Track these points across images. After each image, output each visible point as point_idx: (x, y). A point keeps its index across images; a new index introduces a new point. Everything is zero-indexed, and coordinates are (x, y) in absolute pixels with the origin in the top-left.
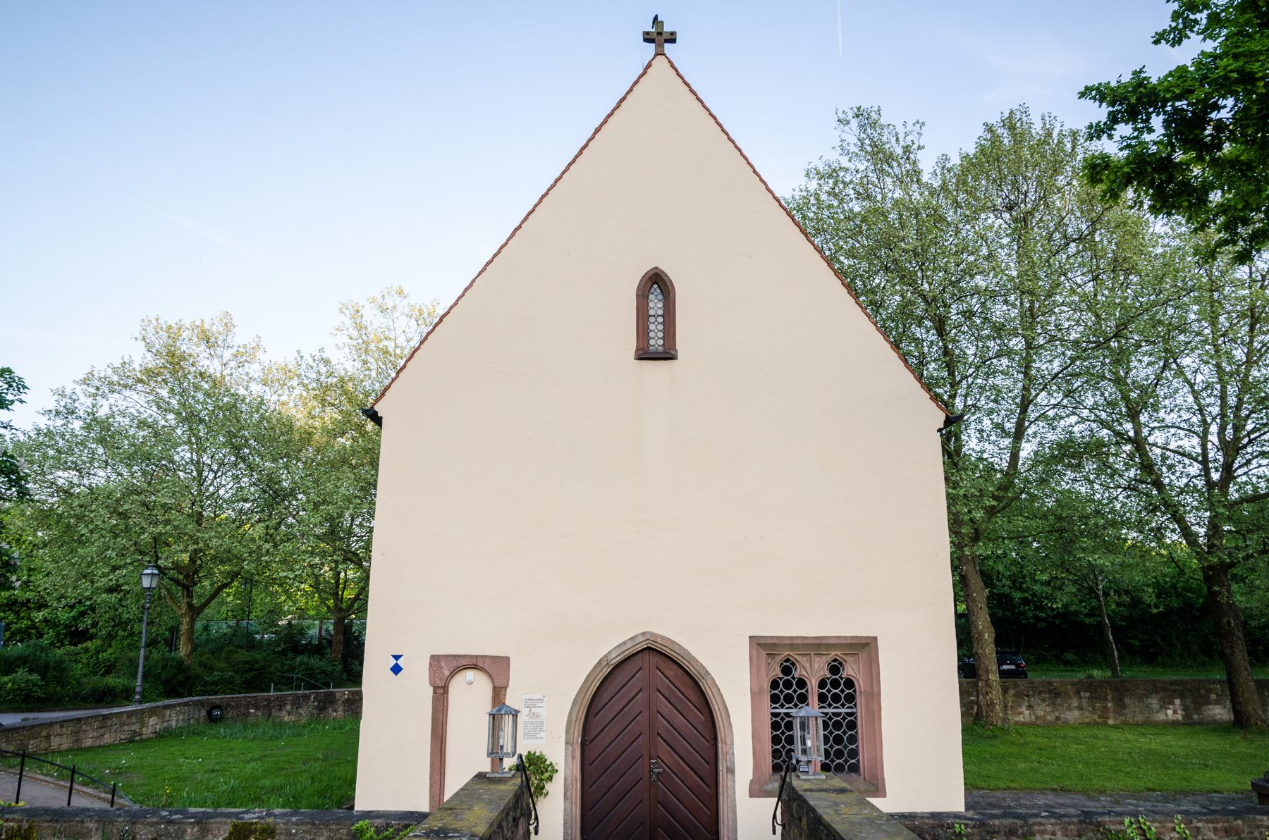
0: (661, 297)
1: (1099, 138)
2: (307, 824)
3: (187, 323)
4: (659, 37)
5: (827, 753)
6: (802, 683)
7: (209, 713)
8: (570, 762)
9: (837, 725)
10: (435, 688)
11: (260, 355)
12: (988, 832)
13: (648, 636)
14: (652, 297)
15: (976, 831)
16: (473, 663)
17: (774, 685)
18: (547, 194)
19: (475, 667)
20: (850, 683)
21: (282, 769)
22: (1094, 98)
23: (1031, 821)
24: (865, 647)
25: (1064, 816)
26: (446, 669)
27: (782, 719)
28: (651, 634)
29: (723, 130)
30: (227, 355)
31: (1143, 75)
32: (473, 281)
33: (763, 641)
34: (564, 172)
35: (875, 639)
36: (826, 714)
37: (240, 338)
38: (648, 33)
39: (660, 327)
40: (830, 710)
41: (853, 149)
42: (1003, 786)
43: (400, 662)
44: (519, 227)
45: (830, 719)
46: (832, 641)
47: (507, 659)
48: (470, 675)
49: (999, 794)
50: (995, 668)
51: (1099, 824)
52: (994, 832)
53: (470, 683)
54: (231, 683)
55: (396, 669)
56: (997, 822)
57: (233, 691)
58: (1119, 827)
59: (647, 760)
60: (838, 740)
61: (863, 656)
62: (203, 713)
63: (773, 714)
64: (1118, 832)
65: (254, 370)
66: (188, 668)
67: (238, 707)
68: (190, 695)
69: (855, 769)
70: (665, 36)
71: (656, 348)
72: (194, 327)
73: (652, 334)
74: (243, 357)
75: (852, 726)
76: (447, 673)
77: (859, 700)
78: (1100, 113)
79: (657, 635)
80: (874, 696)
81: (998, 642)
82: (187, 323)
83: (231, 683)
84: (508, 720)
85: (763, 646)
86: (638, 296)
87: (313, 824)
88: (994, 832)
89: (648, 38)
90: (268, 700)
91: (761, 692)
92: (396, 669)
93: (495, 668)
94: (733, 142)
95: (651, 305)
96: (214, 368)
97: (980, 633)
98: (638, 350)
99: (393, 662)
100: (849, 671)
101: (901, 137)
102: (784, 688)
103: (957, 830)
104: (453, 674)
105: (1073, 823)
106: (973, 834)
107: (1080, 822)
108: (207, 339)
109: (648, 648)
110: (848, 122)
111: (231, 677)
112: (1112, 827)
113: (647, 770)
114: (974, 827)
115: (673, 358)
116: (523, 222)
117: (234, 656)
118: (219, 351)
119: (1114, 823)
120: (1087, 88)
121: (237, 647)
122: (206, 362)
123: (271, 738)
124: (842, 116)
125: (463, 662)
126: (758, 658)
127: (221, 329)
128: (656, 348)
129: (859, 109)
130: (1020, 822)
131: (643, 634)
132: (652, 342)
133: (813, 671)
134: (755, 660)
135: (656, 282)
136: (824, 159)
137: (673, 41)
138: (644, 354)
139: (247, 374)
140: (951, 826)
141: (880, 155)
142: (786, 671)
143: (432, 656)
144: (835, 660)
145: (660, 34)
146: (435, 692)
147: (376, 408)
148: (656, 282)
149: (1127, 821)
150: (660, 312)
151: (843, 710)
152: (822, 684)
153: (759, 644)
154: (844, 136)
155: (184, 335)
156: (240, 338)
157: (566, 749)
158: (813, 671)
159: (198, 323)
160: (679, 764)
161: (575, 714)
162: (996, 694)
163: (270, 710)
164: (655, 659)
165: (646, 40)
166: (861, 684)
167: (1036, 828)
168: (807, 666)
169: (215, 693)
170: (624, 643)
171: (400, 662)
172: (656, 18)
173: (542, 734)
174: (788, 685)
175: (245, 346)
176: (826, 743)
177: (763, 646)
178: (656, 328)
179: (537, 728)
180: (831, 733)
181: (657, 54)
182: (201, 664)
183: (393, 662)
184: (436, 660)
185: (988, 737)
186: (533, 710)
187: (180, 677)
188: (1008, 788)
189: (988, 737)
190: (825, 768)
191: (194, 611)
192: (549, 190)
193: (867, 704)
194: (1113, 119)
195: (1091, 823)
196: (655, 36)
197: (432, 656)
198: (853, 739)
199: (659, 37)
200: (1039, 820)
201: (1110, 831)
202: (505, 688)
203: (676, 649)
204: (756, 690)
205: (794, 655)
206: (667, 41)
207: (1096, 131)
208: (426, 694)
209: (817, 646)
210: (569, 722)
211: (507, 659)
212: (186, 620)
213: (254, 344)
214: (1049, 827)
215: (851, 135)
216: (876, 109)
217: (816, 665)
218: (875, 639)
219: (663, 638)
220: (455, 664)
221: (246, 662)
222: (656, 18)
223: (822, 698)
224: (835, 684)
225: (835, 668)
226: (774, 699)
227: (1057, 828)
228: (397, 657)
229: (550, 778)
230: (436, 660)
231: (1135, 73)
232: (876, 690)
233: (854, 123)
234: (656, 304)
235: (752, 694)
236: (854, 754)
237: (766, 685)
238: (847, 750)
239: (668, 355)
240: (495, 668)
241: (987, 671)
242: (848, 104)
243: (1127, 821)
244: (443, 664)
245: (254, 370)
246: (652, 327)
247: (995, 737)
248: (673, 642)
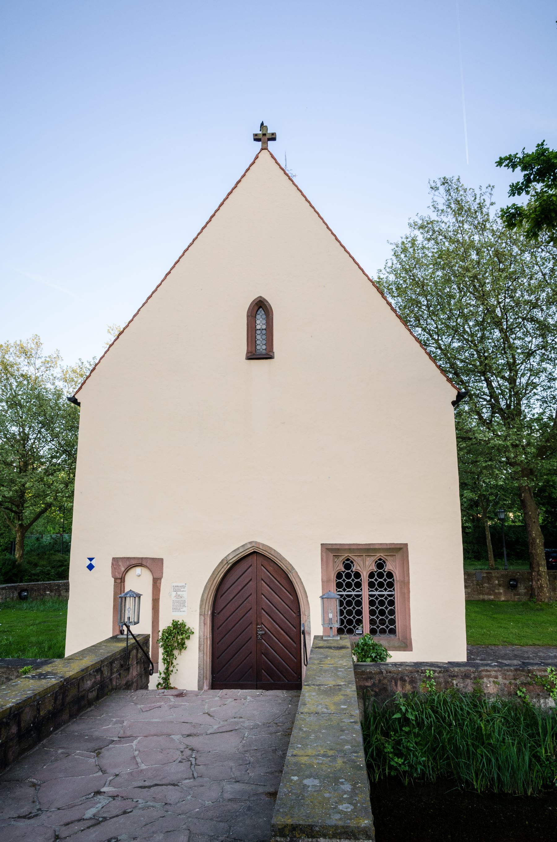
0: (264, 316)
1: (519, 194)
2: (4, 667)
3: (12, 342)
4: (264, 137)
5: (342, 622)
6: (358, 575)
7: (20, 594)
8: (202, 627)
9: (349, 603)
10: (116, 579)
11: (59, 362)
12: (450, 676)
13: (253, 544)
14: (258, 317)
15: (441, 675)
16: (140, 563)
17: (339, 576)
18: (187, 249)
19: (141, 565)
20: (390, 575)
21: (51, 630)
22: (507, 165)
23: (482, 668)
24: (400, 550)
25: (506, 665)
26: (122, 567)
27: (386, 598)
28: (256, 542)
29: (307, 200)
30: (38, 363)
31: (545, 147)
32: (139, 310)
33: (330, 547)
34: (199, 234)
35: (406, 545)
36: (342, 596)
37: (46, 351)
38: (256, 135)
39: (264, 337)
40: (377, 593)
41: (441, 207)
42: (531, 643)
43: (93, 562)
44: (169, 273)
45: (345, 599)
46: (377, 547)
47: (162, 560)
48: (138, 570)
49: (525, 649)
50: (544, 562)
51: (529, 671)
52: (454, 676)
53: (139, 576)
54: (49, 574)
55: (91, 567)
56: (456, 669)
57: (49, 579)
58: (543, 673)
59: (254, 626)
60: (349, 613)
61: (398, 556)
62: (16, 594)
63: (370, 595)
64: (542, 677)
65: (57, 372)
66: (20, 565)
67: (39, 589)
68: (21, 582)
69: (393, 631)
70: (268, 136)
71: (260, 350)
72: (16, 345)
73: (258, 342)
74: (49, 364)
75: (392, 603)
76: (123, 569)
77: (397, 586)
78: (518, 176)
79: (259, 543)
80: (406, 584)
81: (546, 545)
82: (12, 342)
83: (49, 574)
84: (130, 603)
85: (330, 551)
86: (248, 316)
87: (8, 668)
88: (454, 676)
89: (257, 139)
90: (59, 586)
91: (328, 581)
92: (91, 567)
93: (154, 566)
94: (313, 208)
95: (258, 322)
96: (31, 371)
97: (534, 539)
98: (248, 353)
99: (88, 562)
100: (389, 567)
101: (478, 196)
102: (345, 578)
103: (428, 674)
104: (127, 570)
105: (511, 671)
106: (439, 677)
107: (516, 670)
108: (25, 352)
109: (254, 552)
110: (438, 189)
111: (49, 570)
112: (539, 674)
113: (255, 632)
114: (440, 672)
115: (271, 358)
116: (171, 269)
117: (53, 556)
118: (33, 360)
119: (540, 671)
120: (501, 159)
121: (55, 551)
122: (26, 368)
123: (55, 610)
124: (433, 185)
125: (133, 562)
126: (327, 558)
127: (33, 346)
128: (260, 350)
129: (444, 178)
130: (473, 669)
131: (251, 543)
132: (258, 347)
133: (365, 567)
134: (324, 558)
135: (260, 306)
136: (419, 215)
137: (274, 139)
138: (253, 355)
139: (52, 375)
140: (424, 672)
141: (460, 210)
142: (348, 566)
143: (113, 558)
144: (380, 559)
145: (264, 135)
146: (115, 582)
147: (76, 397)
148: (260, 306)
149: (549, 670)
150: (264, 327)
151: (386, 593)
152: (371, 575)
153: (328, 549)
154: (436, 199)
155: (11, 350)
156: (46, 351)
157: (200, 619)
158: (365, 567)
159: (18, 343)
160: (276, 629)
161: (206, 595)
162: (544, 581)
163: (60, 591)
164: (260, 559)
165: (255, 140)
166: (397, 576)
167: (484, 673)
168: (361, 563)
169: (38, 581)
170: (238, 549)
171: (93, 562)
172: (262, 124)
173: (184, 609)
174: (348, 576)
175: (50, 357)
176: (341, 615)
177: (330, 551)
178: (260, 338)
179: (179, 604)
180: (345, 608)
181: (262, 149)
182: (29, 563)
183: (88, 562)
184: (116, 561)
185: (538, 610)
186: (179, 593)
187: (15, 571)
188: (534, 645)
189: (538, 610)
190: (340, 631)
191: (24, 529)
192: (189, 247)
193: (401, 588)
194: (528, 180)
195: (523, 671)
196: (261, 137)
197: (113, 558)
198: (392, 612)
199: (264, 137)
200: (488, 668)
201: (536, 676)
202: (160, 579)
203: (272, 553)
204: (325, 579)
205: (352, 556)
206: (269, 139)
207: (516, 190)
208: (111, 582)
209: (367, 550)
210: (202, 601)
211: (162, 560)
212: (19, 534)
213: (55, 356)
214: (493, 673)
215: (441, 198)
216: (457, 178)
217: (367, 563)
218: (406, 545)
219: (263, 545)
220: (128, 563)
221: (59, 561)
222: (262, 124)
223: (371, 585)
224: (380, 575)
225: (380, 565)
226: (339, 585)
227: (499, 673)
228: (91, 559)
229: (188, 638)
230: (116, 561)
231: (538, 146)
232: (406, 579)
233: (442, 189)
234: (261, 323)
235: (323, 582)
236: (393, 622)
237: (333, 576)
238: (387, 618)
239: (268, 356)
240: (154, 566)
241: (539, 565)
242: (436, 176)
243: (549, 670)
244: (120, 563)
245: (57, 372)
246: (258, 337)
247: (542, 610)
248: (270, 548)
